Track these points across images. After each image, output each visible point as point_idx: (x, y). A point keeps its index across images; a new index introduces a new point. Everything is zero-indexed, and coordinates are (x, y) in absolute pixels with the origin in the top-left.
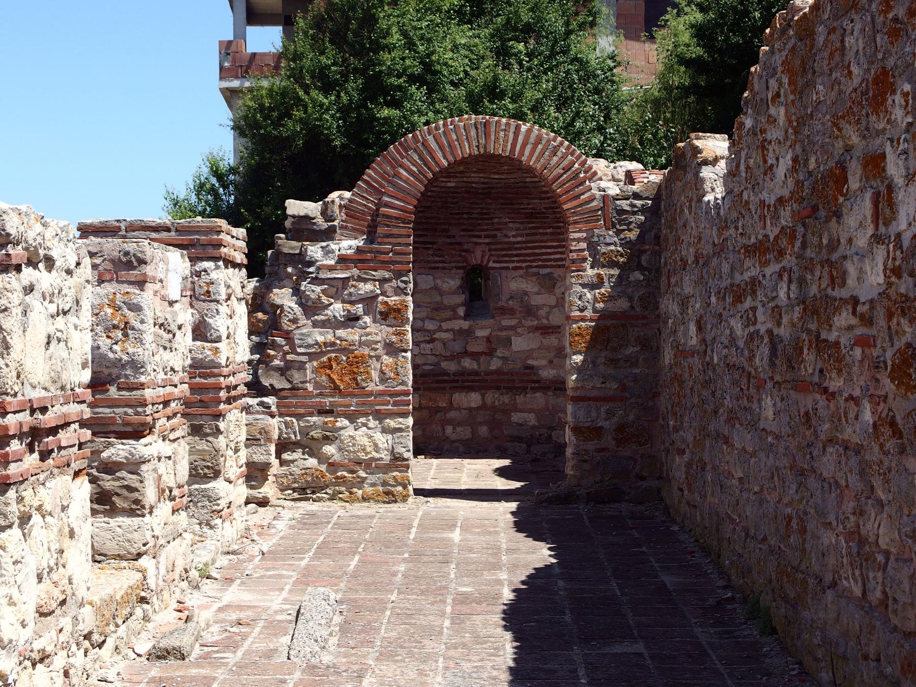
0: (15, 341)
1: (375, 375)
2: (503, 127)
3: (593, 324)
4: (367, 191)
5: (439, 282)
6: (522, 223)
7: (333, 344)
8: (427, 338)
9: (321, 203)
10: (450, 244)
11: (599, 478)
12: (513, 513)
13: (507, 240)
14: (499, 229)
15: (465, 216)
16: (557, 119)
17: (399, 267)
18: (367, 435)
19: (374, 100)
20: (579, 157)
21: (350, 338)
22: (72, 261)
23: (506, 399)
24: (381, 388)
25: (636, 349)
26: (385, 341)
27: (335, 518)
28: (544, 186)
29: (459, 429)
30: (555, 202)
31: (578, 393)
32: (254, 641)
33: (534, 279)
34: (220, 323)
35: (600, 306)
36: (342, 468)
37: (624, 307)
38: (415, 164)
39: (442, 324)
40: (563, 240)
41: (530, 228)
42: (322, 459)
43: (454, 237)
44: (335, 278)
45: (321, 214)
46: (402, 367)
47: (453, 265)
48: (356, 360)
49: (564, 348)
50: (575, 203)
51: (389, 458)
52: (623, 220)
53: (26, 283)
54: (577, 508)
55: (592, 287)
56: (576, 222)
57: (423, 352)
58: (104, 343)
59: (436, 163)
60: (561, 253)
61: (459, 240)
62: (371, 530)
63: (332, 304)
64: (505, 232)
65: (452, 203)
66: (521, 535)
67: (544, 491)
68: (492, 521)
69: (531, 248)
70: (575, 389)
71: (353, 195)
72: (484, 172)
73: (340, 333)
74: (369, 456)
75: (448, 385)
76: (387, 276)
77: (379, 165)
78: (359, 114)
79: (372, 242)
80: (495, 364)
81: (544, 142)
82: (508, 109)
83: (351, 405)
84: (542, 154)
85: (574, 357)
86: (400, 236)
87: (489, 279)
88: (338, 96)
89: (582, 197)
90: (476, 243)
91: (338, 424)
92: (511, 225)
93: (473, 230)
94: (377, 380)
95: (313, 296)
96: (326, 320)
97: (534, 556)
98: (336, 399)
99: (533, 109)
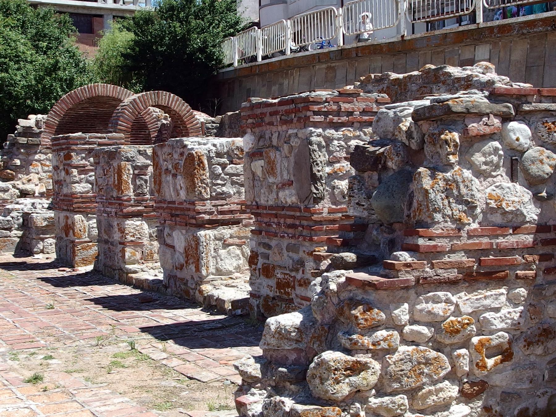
4: (54, 116)
71: (48, 117)
84: (179, 105)
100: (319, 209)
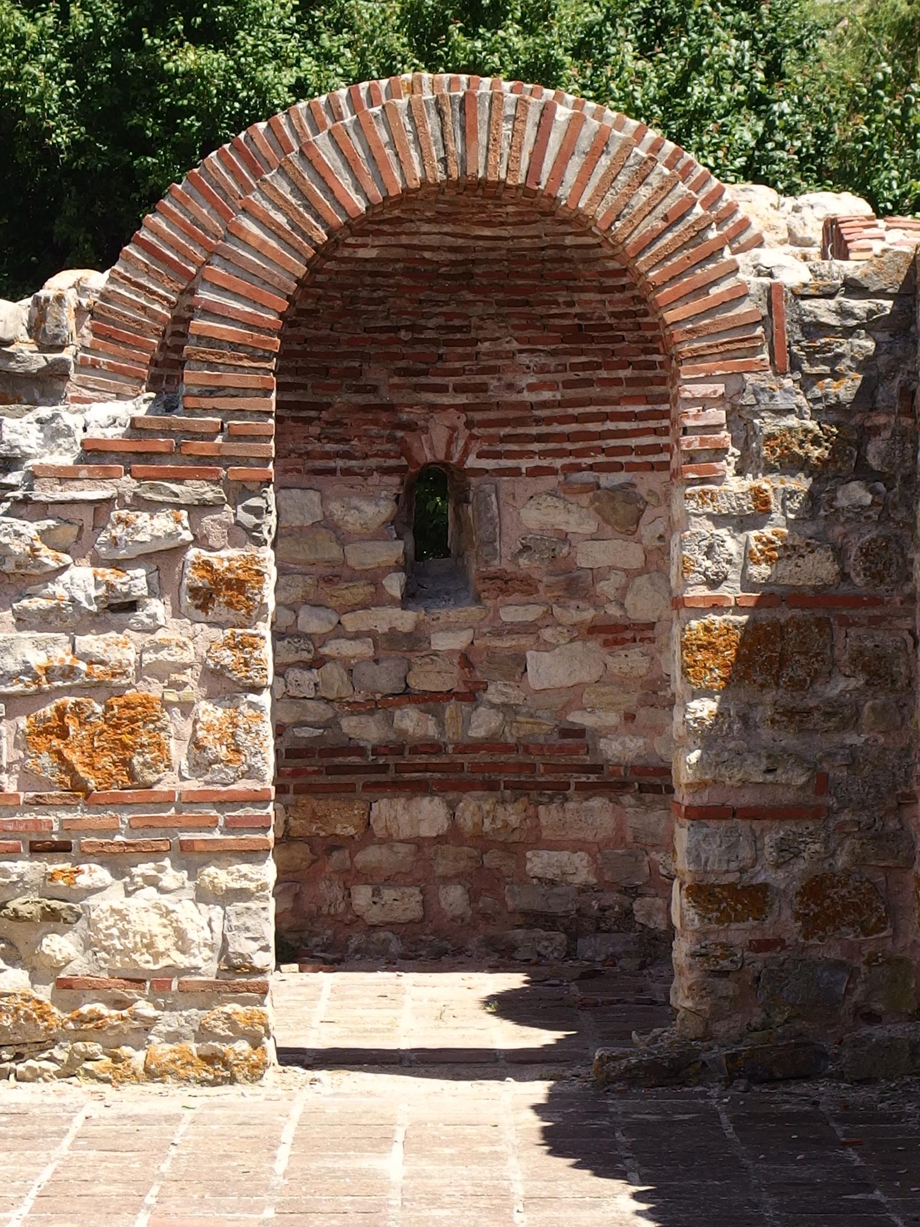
1: (178, 752)
2: (509, 111)
3: (744, 618)
4: (148, 272)
5: (335, 508)
6: (553, 353)
7: (69, 672)
8: (306, 656)
9: (28, 301)
10: (366, 408)
11: (757, 1019)
12: (537, 1109)
13: (514, 397)
14: (492, 370)
15: (403, 334)
16: (641, 76)
17: (240, 472)
18: (157, 907)
19: (159, 25)
20: (703, 182)
21: (114, 656)
23: (512, 814)
24: (194, 785)
25: (853, 683)
26: (204, 663)
27: (79, 1120)
28: (611, 258)
29: (388, 894)
30: (642, 300)
31: (704, 798)
33: (585, 499)
35: (761, 571)
36: (93, 995)
37: (823, 573)
39: (347, 619)
40: (664, 398)
41: (574, 367)
43: (374, 389)
44: (73, 502)
45: (29, 331)
46: (248, 732)
47: (373, 462)
48: (128, 713)
49: (666, 680)
50: (696, 306)
51: (213, 967)
52: (820, 350)
54: (704, 1095)
56: (697, 356)
57: (293, 692)
59: (337, 202)
60: (655, 432)
61: (387, 397)
62: (173, 1151)
63: (66, 567)
64: (508, 377)
65: (370, 301)
66: (562, 1163)
67: (617, 1051)
68: (484, 1129)
69: (576, 419)
70: (698, 786)
71: (111, 280)
72: (455, 222)
73: (89, 642)
74: (164, 962)
75: (359, 780)
76: (209, 496)
77: (181, 202)
78: (119, 64)
79: (170, 408)
81: (614, 149)
82: (512, 52)
83: (117, 831)
84: (610, 178)
85: (695, 705)
86: (244, 392)
87: (467, 501)
88: (64, 16)
89: (714, 291)
90: (433, 407)
91: (83, 881)
92: (524, 359)
93: (425, 373)
94: (185, 764)
95: (18, 547)
96: (50, 611)
97: (597, 1213)
98: (78, 815)
99: (579, 51)
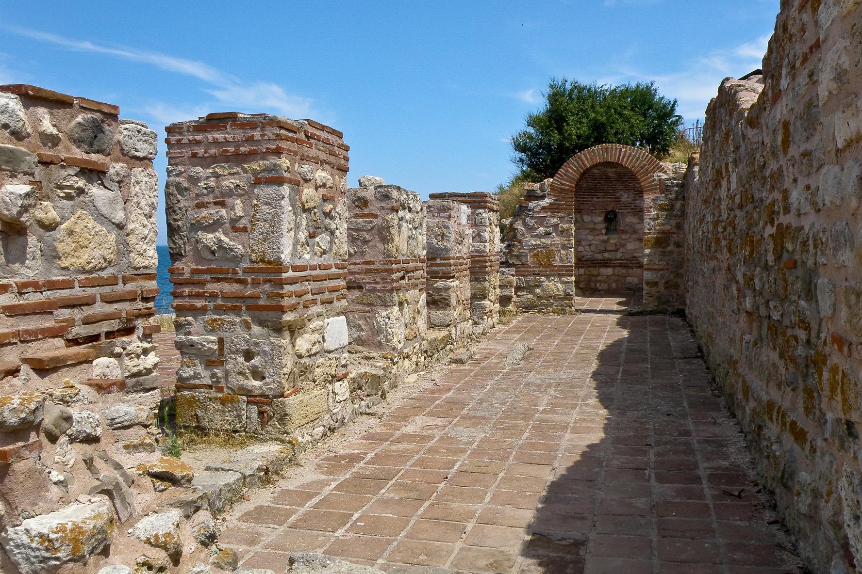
0: (396, 238)
7: (539, 245)
21: (547, 242)
22: (419, 209)
23: (624, 271)
29: (602, 285)
32: (493, 360)
34: (486, 235)
38: (575, 167)
42: (535, 294)
53: (400, 216)
55: (654, 219)
58: (435, 241)
73: (543, 240)
80: (619, 255)
100: (178, 269)
